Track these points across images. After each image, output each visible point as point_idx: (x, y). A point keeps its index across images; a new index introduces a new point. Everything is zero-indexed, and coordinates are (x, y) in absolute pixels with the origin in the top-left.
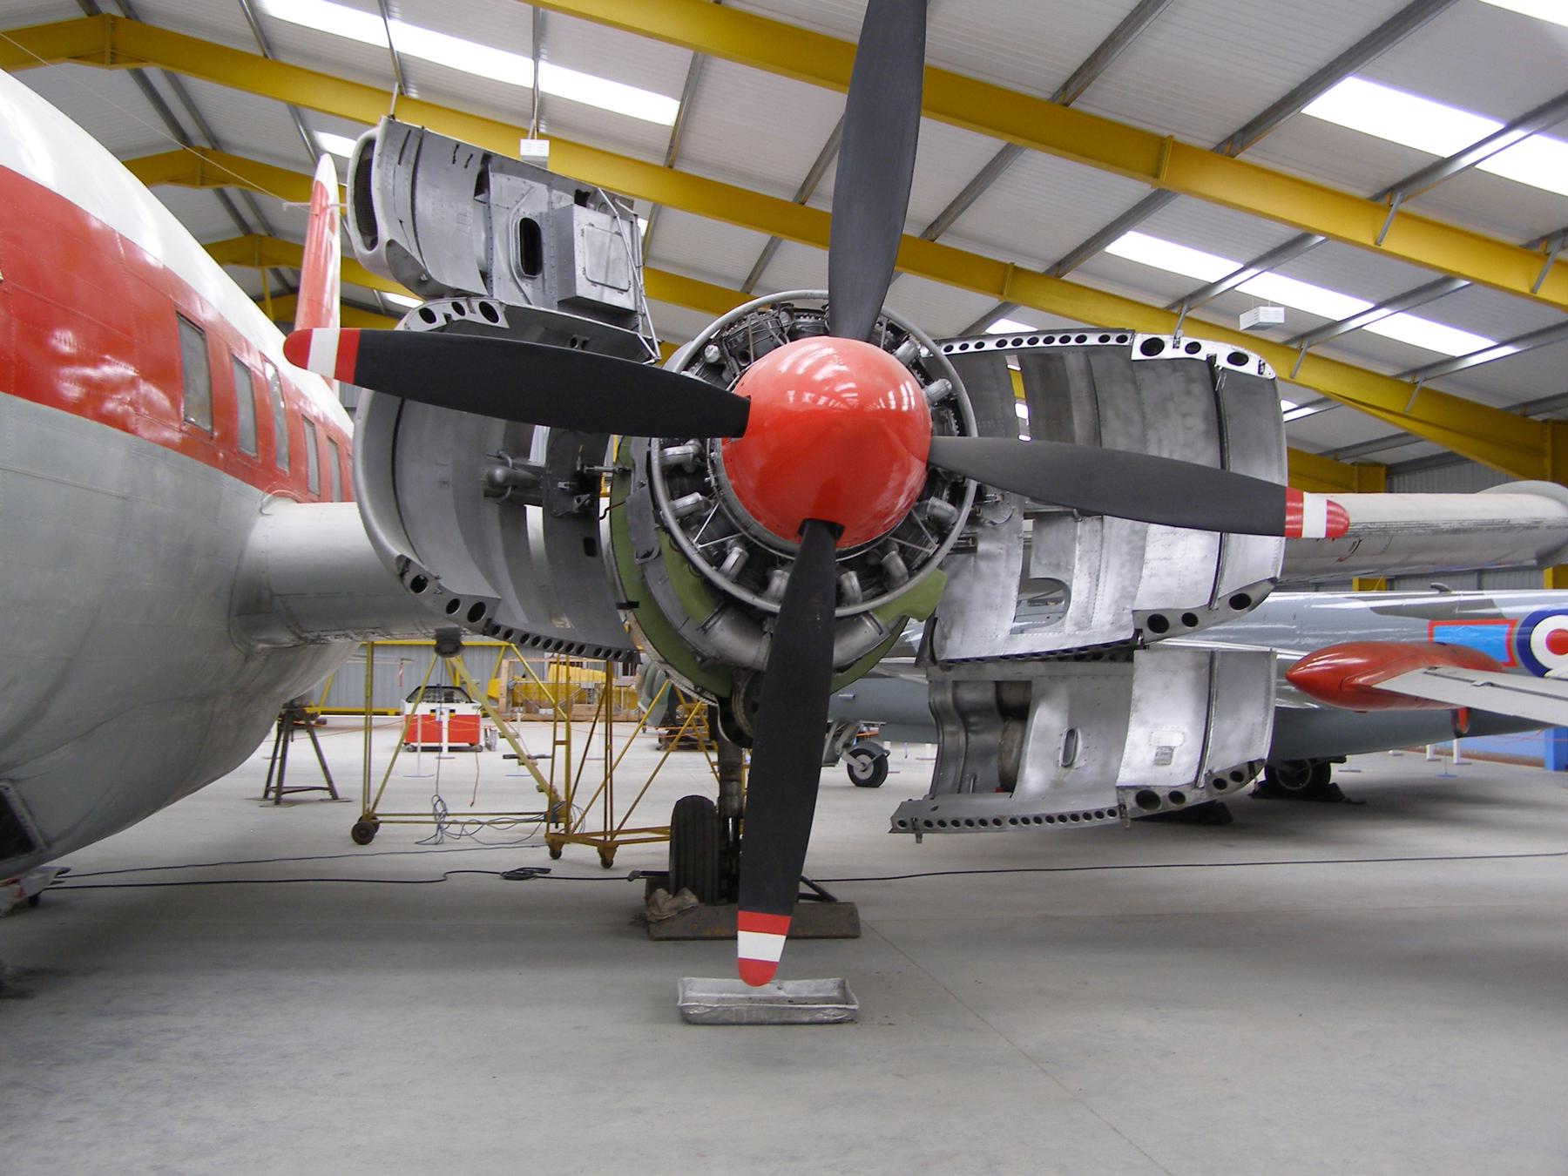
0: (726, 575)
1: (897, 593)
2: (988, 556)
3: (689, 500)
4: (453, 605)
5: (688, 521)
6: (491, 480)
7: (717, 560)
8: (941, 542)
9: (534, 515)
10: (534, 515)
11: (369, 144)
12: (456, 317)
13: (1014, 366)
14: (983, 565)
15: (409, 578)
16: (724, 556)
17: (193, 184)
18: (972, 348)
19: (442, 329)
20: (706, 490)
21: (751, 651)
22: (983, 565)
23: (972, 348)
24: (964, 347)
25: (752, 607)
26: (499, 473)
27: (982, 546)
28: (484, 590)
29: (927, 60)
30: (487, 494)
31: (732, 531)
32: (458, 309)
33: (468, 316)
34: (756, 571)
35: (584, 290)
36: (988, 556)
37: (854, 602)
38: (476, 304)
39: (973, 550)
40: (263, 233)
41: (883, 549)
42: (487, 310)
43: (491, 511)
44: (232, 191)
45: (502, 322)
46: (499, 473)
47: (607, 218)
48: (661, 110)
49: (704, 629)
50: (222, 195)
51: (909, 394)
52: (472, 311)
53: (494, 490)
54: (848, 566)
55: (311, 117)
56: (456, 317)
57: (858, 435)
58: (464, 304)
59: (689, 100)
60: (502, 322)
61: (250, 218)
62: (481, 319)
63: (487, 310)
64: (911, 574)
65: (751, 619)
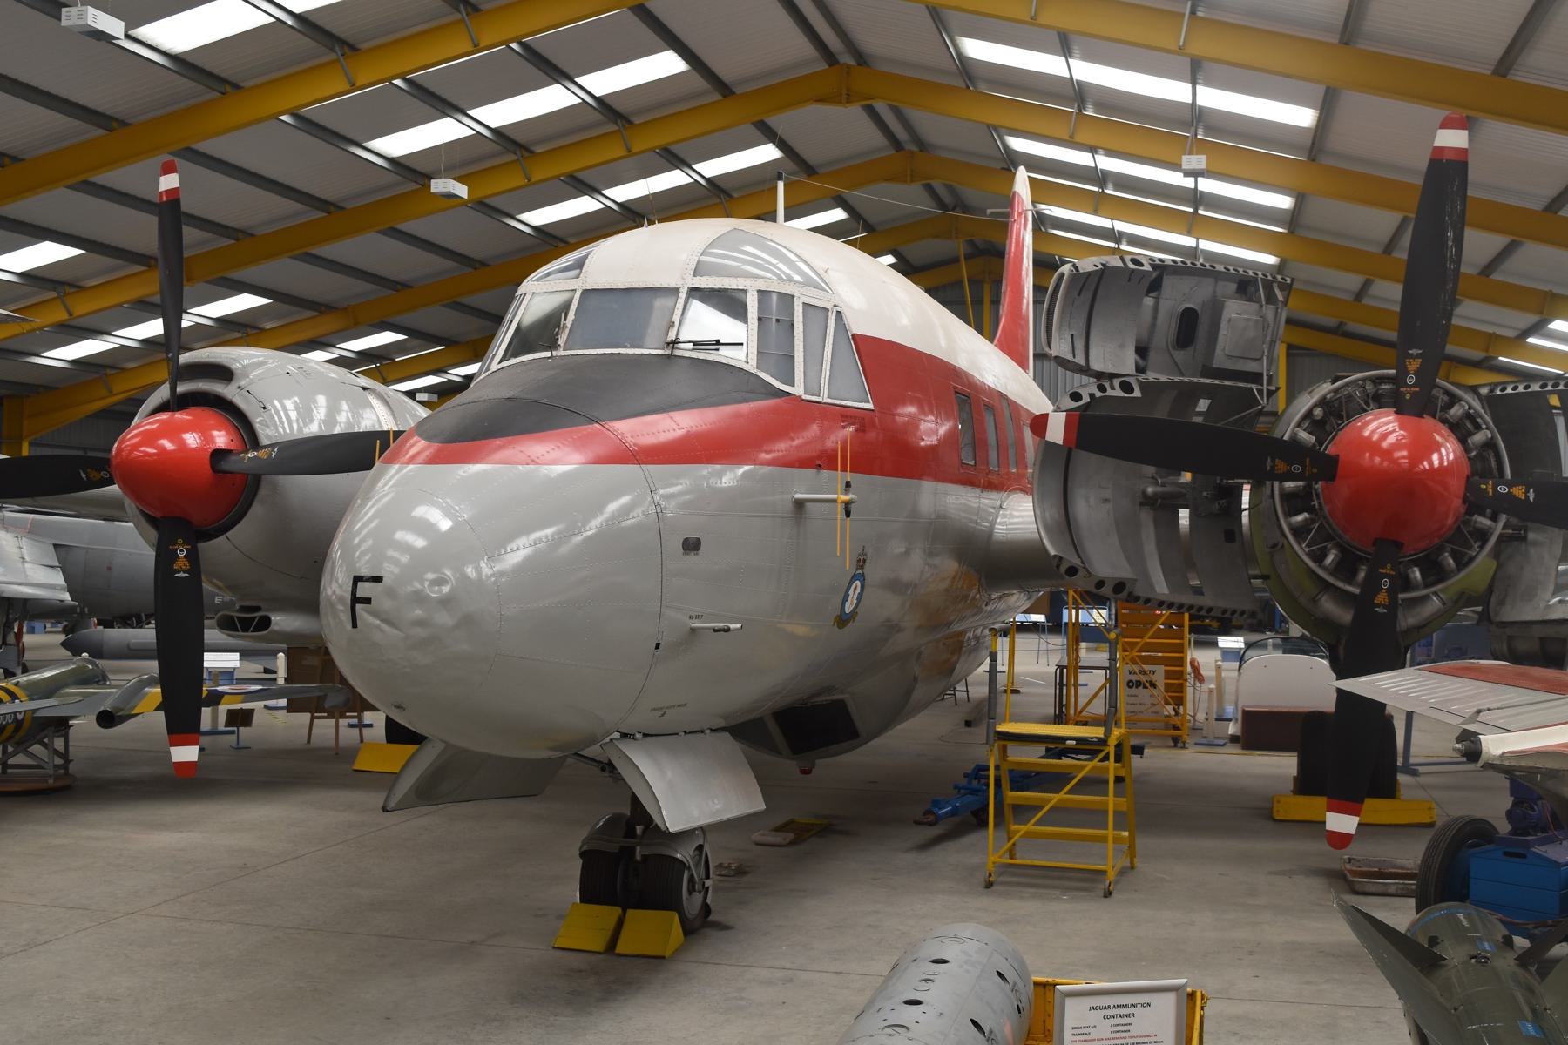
0: (1325, 569)
1: (1449, 582)
2: (1535, 544)
3: (1300, 518)
4: (1100, 584)
5: (1299, 532)
6: (1144, 493)
7: (1319, 558)
8: (1481, 547)
9: (1184, 513)
10: (1184, 513)
11: (994, 632)
12: (1098, 394)
13: (1554, 401)
14: (1532, 551)
15: (1063, 569)
16: (1325, 556)
17: (840, 102)
18: (1521, 389)
19: (1087, 406)
20: (1311, 510)
21: (1345, 616)
22: (1532, 551)
23: (1521, 389)
24: (1515, 388)
25: (1343, 591)
26: (1150, 490)
27: (1531, 536)
28: (1124, 571)
29: (1470, 193)
30: (1142, 504)
31: (1329, 538)
32: (1102, 388)
33: (1110, 393)
34: (1346, 568)
35: (1219, 361)
36: (1535, 544)
37: (1416, 588)
38: (1116, 382)
39: (1524, 539)
40: (914, 148)
41: (1440, 549)
42: (1127, 387)
43: (1146, 517)
44: (881, 107)
45: (1137, 393)
46: (1150, 490)
47: (1255, 306)
48: (1302, 117)
49: (1314, 600)
50: (871, 112)
51: (1446, 452)
52: (1113, 388)
53: (1147, 501)
54: (1415, 563)
55: (953, 18)
56: (1098, 394)
57: (1406, 488)
58: (1107, 385)
59: (1327, 108)
60: (1137, 393)
61: (901, 134)
62: (1118, 393)
63: (1127, 387)
64: (1459, 570)
65: (1343, 597)
